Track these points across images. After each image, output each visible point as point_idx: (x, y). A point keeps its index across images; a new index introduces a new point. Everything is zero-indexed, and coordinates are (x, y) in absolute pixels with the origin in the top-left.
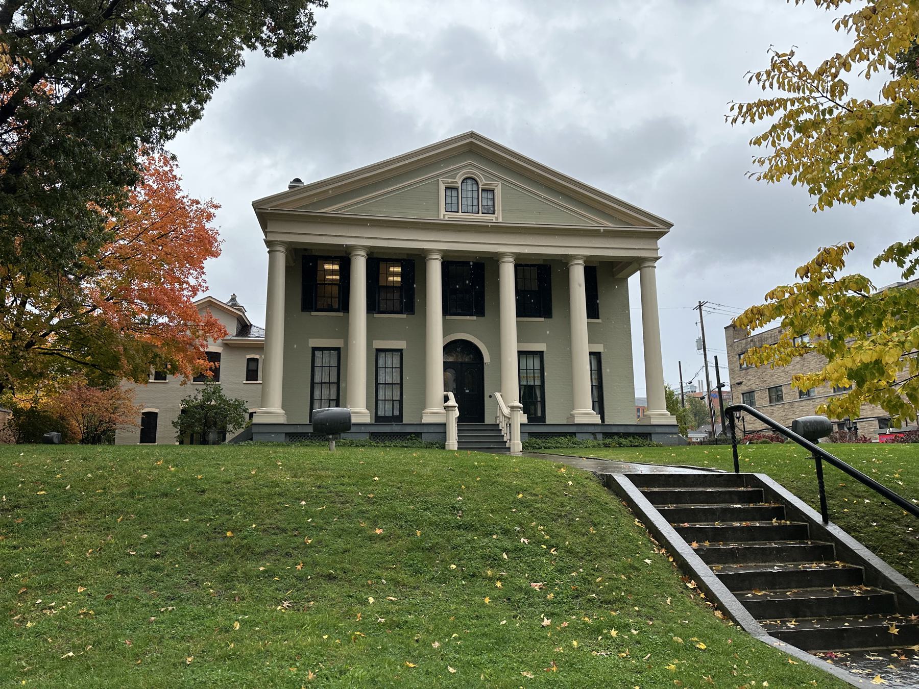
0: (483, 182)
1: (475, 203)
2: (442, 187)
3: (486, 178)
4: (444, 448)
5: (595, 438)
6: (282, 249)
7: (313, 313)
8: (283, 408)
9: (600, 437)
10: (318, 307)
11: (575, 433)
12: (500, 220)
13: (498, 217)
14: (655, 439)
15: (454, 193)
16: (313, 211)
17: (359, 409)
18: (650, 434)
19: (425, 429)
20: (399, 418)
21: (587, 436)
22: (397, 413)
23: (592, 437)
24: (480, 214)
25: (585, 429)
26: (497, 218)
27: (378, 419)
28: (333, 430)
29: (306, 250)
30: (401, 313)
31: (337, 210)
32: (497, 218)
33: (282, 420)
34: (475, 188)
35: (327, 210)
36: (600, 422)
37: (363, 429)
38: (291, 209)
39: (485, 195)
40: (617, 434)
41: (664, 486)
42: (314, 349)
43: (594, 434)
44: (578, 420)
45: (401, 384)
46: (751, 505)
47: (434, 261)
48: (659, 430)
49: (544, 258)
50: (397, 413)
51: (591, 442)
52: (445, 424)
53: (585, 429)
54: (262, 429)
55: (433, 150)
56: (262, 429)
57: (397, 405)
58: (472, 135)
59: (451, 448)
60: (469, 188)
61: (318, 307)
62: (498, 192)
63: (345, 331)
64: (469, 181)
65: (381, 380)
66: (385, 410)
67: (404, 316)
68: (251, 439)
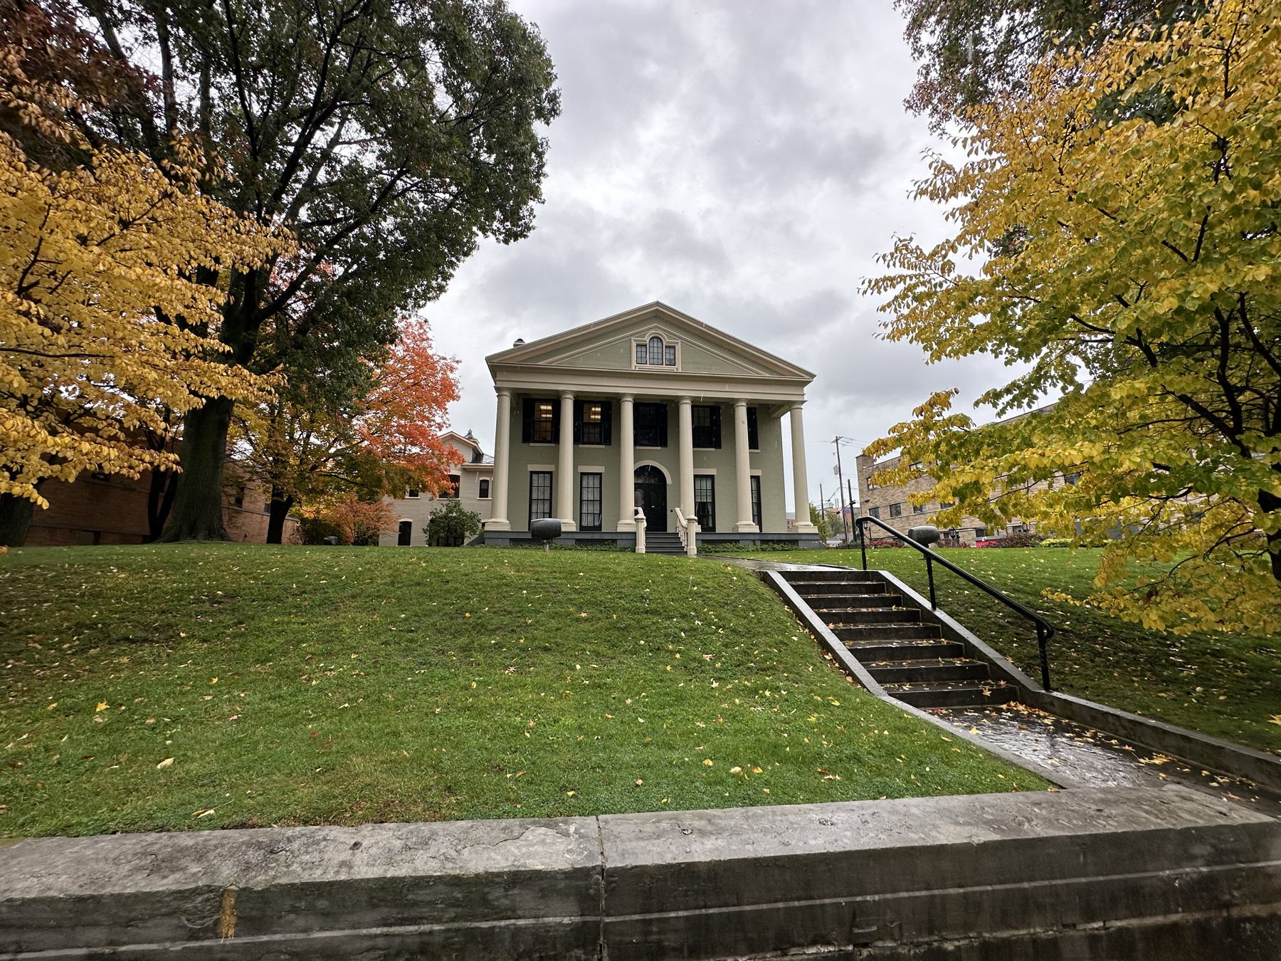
2: (634, 344)
9: (758, 543)
13: (678, 368)
16: (531, 364)
17: (567, 520)
22: (597, 524)
27: (583, 529)
28: (545, 536)
33: (507, 528)
37: (503, 536)
38: (514, 362)
42: (532, 473)
45: (600, 501)
53: (503, 536)
58: (658, 304)
62: (678, 348)
63: (556, 458)
65: (534, 496)
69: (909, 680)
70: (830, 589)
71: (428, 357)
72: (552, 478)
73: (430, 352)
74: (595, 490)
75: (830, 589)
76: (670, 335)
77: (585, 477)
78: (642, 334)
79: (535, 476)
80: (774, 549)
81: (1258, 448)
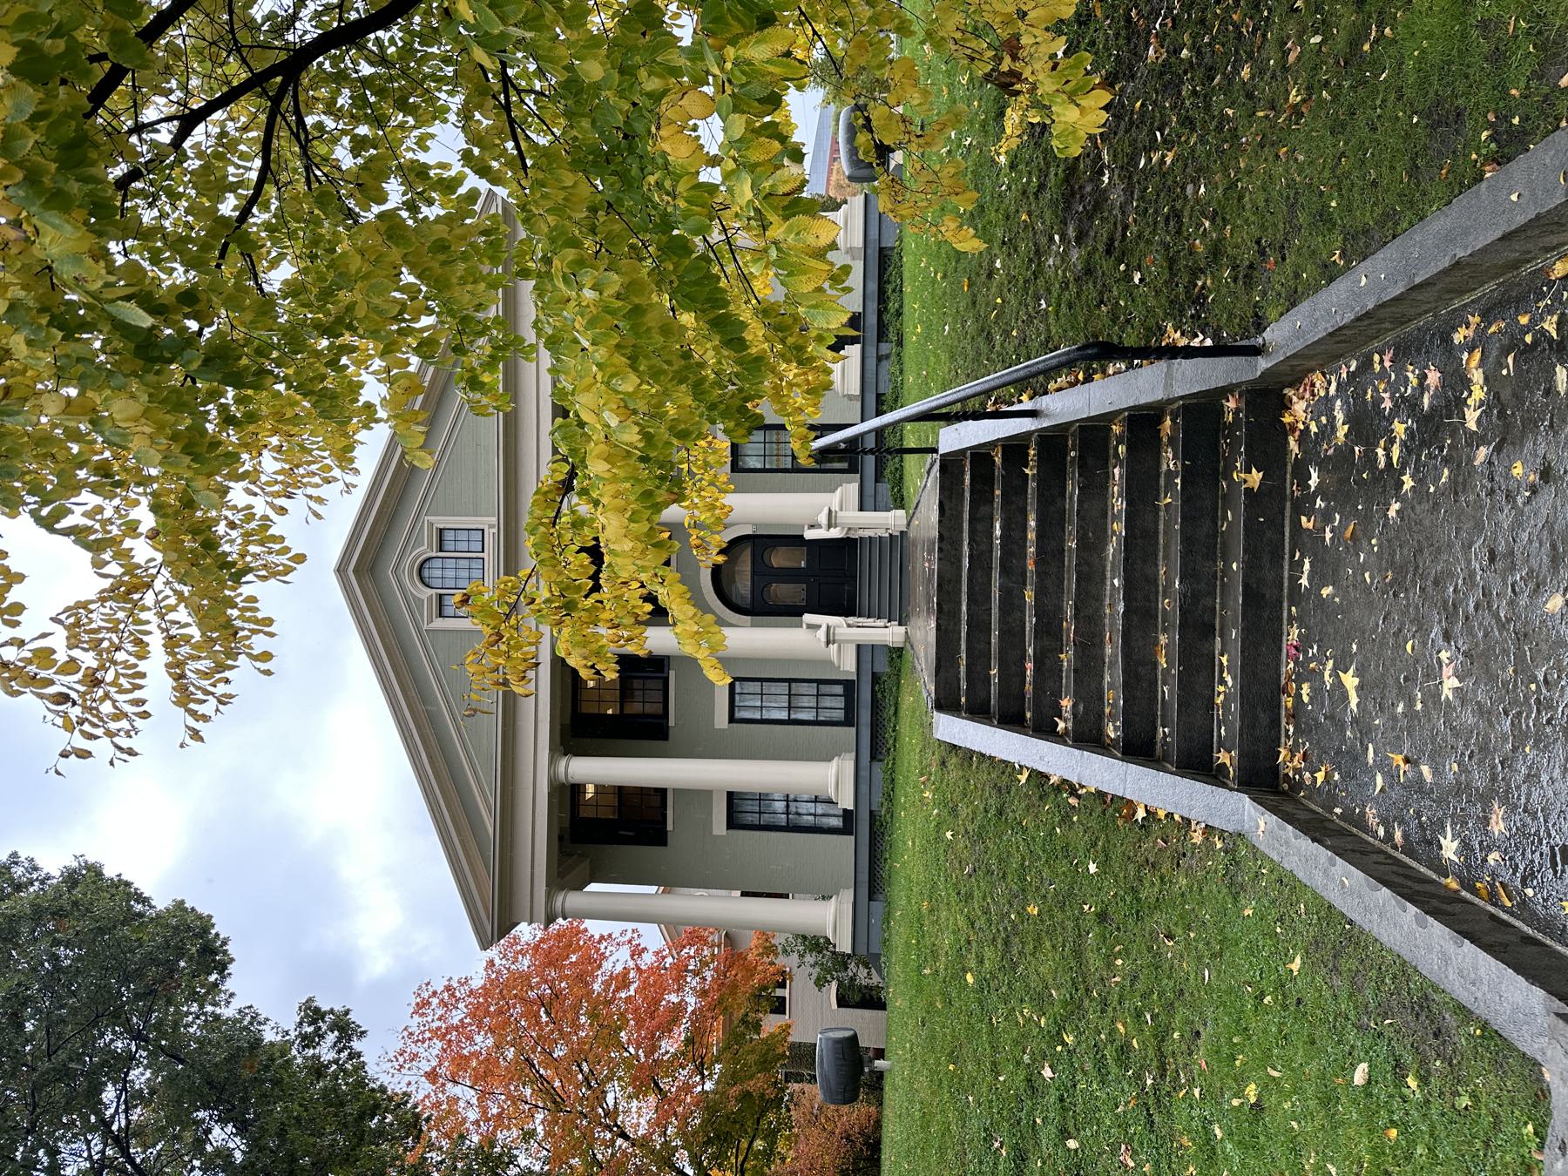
0: (426, 549)
1: (465, 563)
2: (439, 623)
3: (418, 543)
4: (901, 650)
5: (887, 357)
6: (560, 899)
7: (670, 827)
8: (830, 760)
9: (885, 348)
10: (660, 711)
11: (879, 396)
12: (494, 520)
13: (490, 522)
14: (888, 243)
15: (449, 536)
16: (493, 851)
17: (830, 777)
18: (881, 250)
19: (867, 667)
20: (849, 687)
21: (883, 372)
22: (839, 689)
23: (884, 363)
24: (484, 555)
25: (871, 375)
26: (491, 526)
27: (849, 720)
28: (869, 828)
29: (561, 838)
30: (666, 681)
31: (486, 801)
32: (491, 526)
33: (849, 765)
34: (438, 563)
35: (489, 824)
36: (858, 347)
37: (864, 773)
38: (490, 886)
39: (449, 545)
40: (880, 314)
41: (961, 532)
42: (732, 719)
43: (880, 359)
44: (855, 389)
45: (790, 681)
46: (998, 492)
47: (570, 770)
48: (874, 233)
49: (558, 700)
50: (839, 689)
51: (889, 367)
52: (858, 646)
53: (871, 375)
54: (862, 938)
55: (370, 511)
56: (862, 938)
57: (825, 689)
58: (341, 570)
59: (902, 639)
60: (438, 573)
61: (660, 711)
62: (441, 521)
63: (698, 796)
64: (426, 573)
65: (783, 715)
66: (834, 706)
67: (672, 674)
68: (878, 956)
69: (1208, 631)
70: (979, 627)
71: (486, 991)
72: (741, 810)
73: (477, 983)
74: (772, 707)
75: (979, 627)
76: (413, 540)
77: (739, 714)
78: (414, 604)
79: (739, 714)
80: (899, 313)
81: (609, 514)
